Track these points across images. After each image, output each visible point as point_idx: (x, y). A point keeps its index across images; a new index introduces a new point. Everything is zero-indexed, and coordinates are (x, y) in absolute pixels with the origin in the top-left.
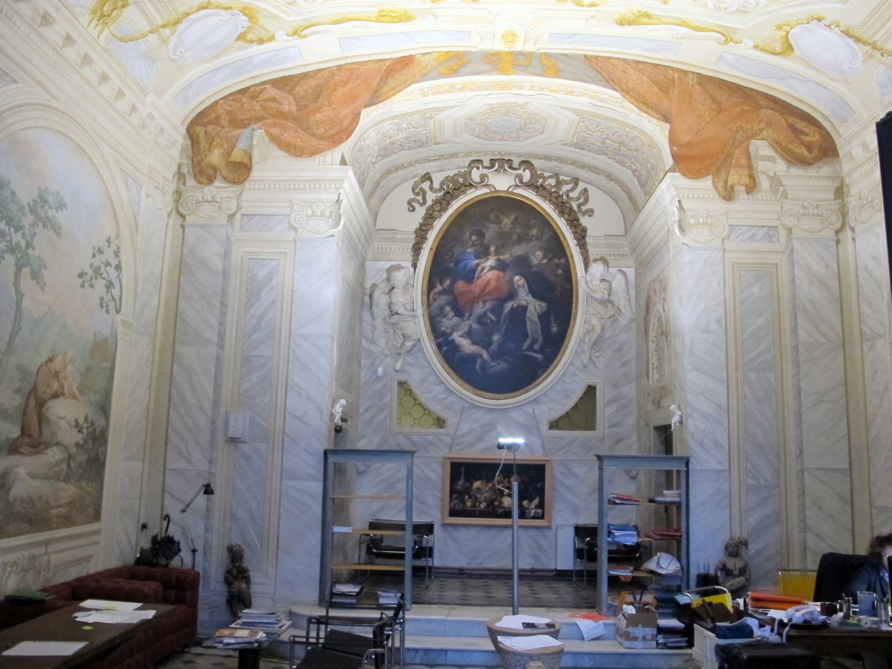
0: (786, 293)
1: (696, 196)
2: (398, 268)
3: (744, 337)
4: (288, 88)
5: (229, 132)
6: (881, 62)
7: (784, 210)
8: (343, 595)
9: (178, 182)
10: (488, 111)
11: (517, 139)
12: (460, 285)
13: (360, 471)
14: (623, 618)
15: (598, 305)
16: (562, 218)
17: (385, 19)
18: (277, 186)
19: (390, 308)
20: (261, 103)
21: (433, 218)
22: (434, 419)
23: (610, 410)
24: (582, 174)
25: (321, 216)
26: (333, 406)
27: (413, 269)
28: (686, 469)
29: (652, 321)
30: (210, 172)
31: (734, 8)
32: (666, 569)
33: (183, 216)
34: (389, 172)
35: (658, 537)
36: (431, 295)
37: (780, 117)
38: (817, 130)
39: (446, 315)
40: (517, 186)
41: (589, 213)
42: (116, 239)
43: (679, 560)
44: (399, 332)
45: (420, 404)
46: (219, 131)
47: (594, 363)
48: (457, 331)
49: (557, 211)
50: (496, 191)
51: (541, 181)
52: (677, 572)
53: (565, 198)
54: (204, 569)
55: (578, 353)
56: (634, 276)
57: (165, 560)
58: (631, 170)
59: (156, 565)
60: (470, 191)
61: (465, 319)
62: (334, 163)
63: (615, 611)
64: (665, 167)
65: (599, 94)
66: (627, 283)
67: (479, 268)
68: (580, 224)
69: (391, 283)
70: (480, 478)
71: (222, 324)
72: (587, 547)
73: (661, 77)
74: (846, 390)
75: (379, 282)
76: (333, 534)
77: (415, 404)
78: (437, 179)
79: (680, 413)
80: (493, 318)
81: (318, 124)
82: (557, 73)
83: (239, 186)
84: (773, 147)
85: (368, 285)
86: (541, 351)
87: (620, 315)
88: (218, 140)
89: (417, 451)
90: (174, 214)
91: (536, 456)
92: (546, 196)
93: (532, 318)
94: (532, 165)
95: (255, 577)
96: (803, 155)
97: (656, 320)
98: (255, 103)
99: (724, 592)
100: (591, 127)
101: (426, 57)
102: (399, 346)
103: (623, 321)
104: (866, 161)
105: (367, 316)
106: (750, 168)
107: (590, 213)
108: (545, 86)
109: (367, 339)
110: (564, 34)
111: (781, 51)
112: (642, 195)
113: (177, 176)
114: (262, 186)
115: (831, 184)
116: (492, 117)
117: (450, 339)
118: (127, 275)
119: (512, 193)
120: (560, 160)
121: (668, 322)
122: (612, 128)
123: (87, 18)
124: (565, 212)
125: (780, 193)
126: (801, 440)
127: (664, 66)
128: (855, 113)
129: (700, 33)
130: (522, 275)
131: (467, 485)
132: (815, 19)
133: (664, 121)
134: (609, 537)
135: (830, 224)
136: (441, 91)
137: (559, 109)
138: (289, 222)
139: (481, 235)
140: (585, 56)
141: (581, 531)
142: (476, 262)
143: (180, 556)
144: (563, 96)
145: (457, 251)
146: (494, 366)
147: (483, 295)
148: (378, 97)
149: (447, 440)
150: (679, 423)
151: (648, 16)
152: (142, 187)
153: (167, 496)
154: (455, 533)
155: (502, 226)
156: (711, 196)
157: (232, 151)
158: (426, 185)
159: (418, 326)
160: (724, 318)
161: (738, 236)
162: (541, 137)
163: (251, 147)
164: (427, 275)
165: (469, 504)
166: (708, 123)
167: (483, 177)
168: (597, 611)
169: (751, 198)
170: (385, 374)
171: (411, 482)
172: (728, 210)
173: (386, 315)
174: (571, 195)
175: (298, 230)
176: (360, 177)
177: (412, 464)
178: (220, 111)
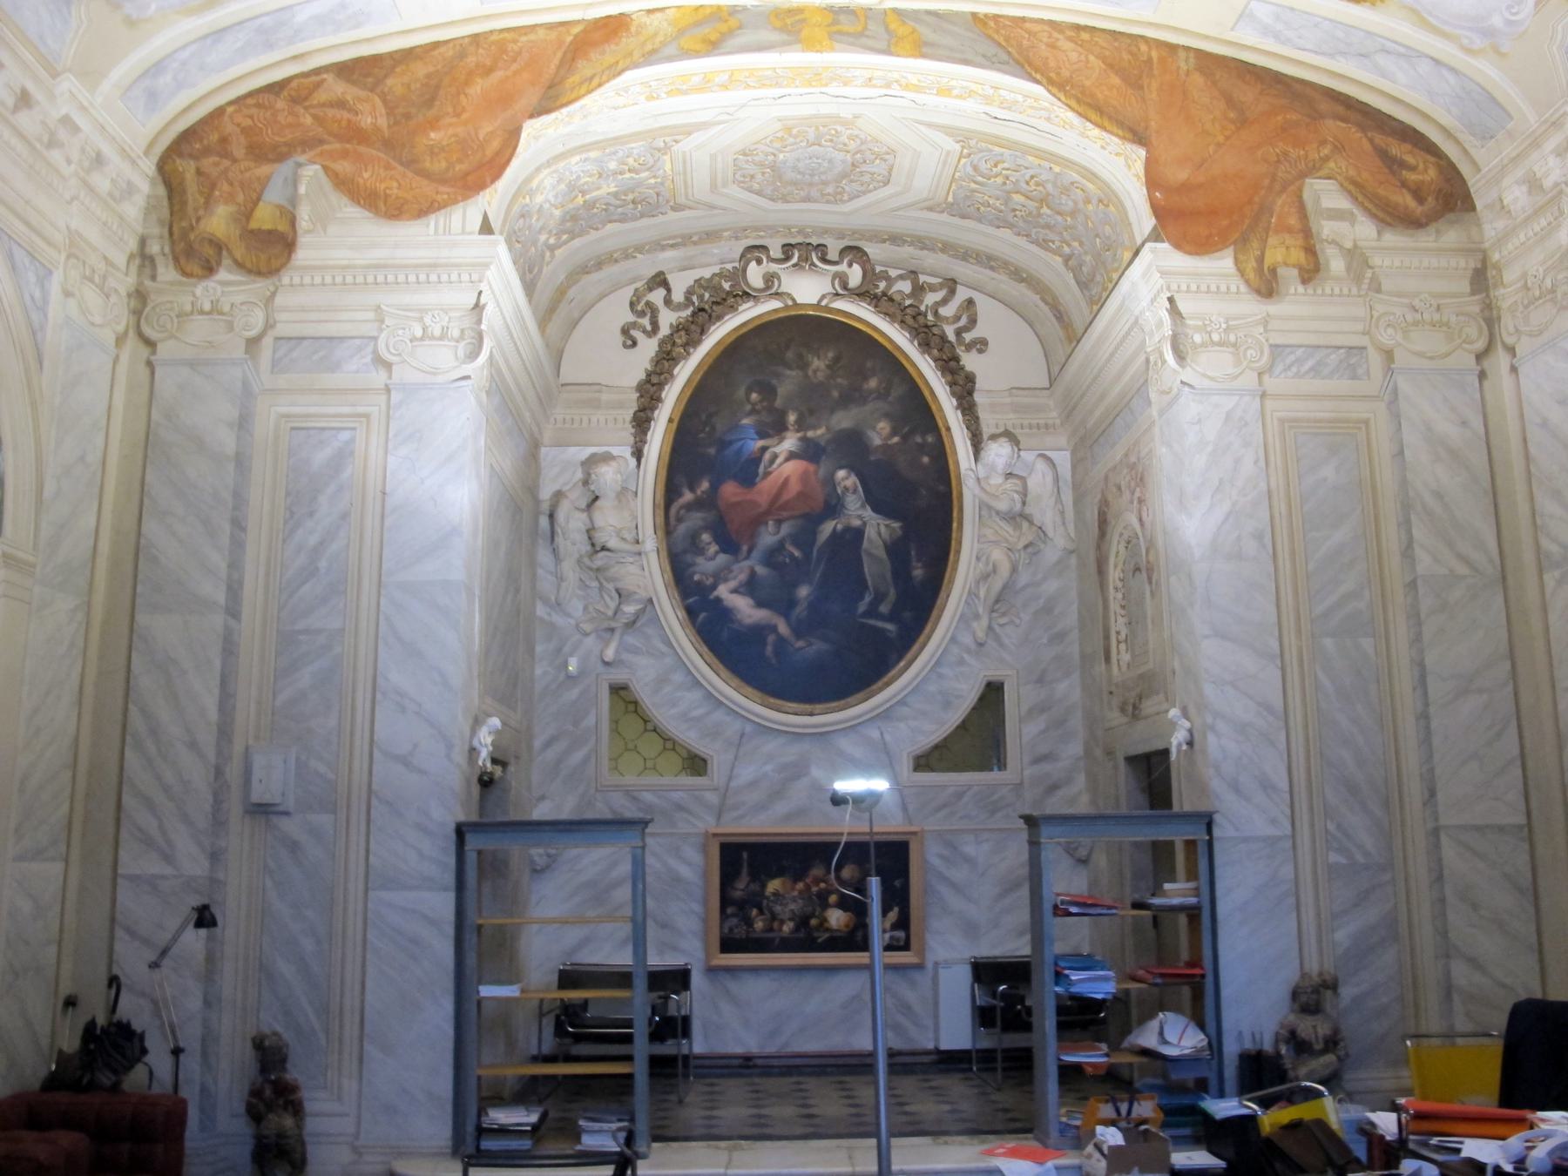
0: (1387, 477)
1: (1204, 288)
2: (607, 458)
3: (1311, 567)
4: (370, 80)
5: (249, 169)
7: (1376, 314)
8: (503, 1131)
9: (139, 275)
10: (779, 135)
11: (837, 198)
12: (730, 490)
13: (539, 868)
14: (1097, 1155)
15: (1003, 524)
16: (926, 356)
19: (590, 538)
20: (312, 111)
21: (673, 359)
22: (683, 759)
23: (1032, 729)
24: (961, 270)
25: (441, 338)
26: (474, 732)
27: (634, 460)
28: (1207, 838)
30: (209, 251)
32: (1177, 1046)
33: (150, 344)
34: (585, 270)
35: (1159, 981)
37: (1359, 135)
38: (1432, 159)
39: (703, 548)
40: (837, 294)
41: (978, 346)
43: (1202, 1026)
44: (610, 586)
45: (655, 730)
47: (998, 639)
48: (726, 580)
49: (916, 343)
50: (796, 304)
51: (882, 285)
52: (1202, 1050)
53: (930, 317)
54: (204, 1090)
55: (965, 620)
56: (1069, 466)
57: (111, 1075)
58: (1060, 256)
59: (92, 1086)
60: (745, 306)
62: (468, 229)
63: (1079, 1139)
64: (1132, 237)
65: (1001, 92)
66: (1057, 479)
67: (767, 456)
68: (962, 368)
69: (592, 488)
70: (780, 873)
71: (235, 565)
72: (1002, 1004)
73: (1126, 56)
75: (567, 488)
76: (479, 1003)
77: (646, 730)
78: (680, 284)
79: (1187, 724)
80: (797, 553)
81: (433, 151)
82: (922, 49)
84: (1350, 192)
85: (546, 494)
86: (892, 617)
88: (226, 187)
89: (651, 821)
90: (132, 341)
91: (890, 824)
92: (894, 313)
93: (874, 551)
94: (865, 254)
95: (316, 1102)
96: (1406, 208)
97: (1123, 544)
98: (302, 111)
99: (1319, 1095)
100: (983, 167)
101: (652, 16)
102: (610, 613)
103: (1051, 555)
105: (544, 556)
106: (1307, 233)
107: (981, 345)
108: (896, 76)
109: (546, 601)
112: (1083, 304)
113: (137, 261)
114: (318, 280)
115: (1462, 263)
116: (788, 149)
117: (712, 597)
119: (828, 309)
120: (922, 243)
121: (1151, 545)
122: (1027, 168)
124: (932, 344)
125: (1367, 281)
126: (1432, 770)
127: (1130, 36)
128: (1509, 115)
130: (851, 468)
131: (754, 887)
133: (1133, 142)
134: (1057, 984)
135: (1464, 341)
136: (684, 87)
137: (922, 128)
138: (375, 352)
139: (768, 391)
140: (974, 15)
141: (985, 972)
142: (761, 443)
143: (146, 1064)
144: (930, 99)
145: (720, 424)
146: (801, 648)
147: (776, 509)
149: (712, 798)
150: (1187, 744)
152: (51, 273)
153: (119, 933)
154: (733, 986)
155: (810, 373)
156: (1233, 289)
157: (252, 210)
158: (657, 296)
159: (647, 573)
160: (1269, 529)
161: (1289, 367)
163: (294, 200)
164: (664, 473)
165: (759, 925)
166: (1219, 145)
167: (770, 279)
168: (1037, 1139)
169: (1310, 291)
170: (582, 672)
171: (641, 886)
172: (1268, 315)
173: (583, 552)
174: (943, 311)
175: (394, 367)
177: (643, 848)
178: (229, 128)
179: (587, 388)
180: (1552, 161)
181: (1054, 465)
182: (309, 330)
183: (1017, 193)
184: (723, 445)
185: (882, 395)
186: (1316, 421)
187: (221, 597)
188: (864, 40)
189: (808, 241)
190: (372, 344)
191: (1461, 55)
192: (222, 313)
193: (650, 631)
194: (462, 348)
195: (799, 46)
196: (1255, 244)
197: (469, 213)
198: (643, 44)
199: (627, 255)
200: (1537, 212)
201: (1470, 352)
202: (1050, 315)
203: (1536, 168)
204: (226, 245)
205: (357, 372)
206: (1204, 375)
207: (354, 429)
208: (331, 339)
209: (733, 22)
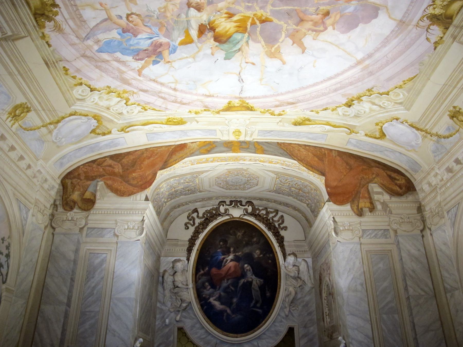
0: (398, 266)
1: (342, 214)
2: (179, 261)
3: (378, 293)
4: (118, 160)
5: (84, 183)
6: (431, 140)
7: (391, 220)
9: (53, 209)
11: (244, 189)
12: (214, 270)
17: (170, 123)
18: (109, 212)
20: (103, 167)
21: (199, 233)
23: (303, 342)
25: (132, 229)
29: (324, 287)
31: (353, 115)
33: (54, 228)
34: (175, 208)
36: (198, 276)
37: (383, 171)
40: (245, 215)
42: (8, 238)
44: (179, 298)
46: (79, 182)
48: (213, 297)
49: (267, 228)
50: (233, 217)
51: (258, 212)
53: (271, 221)
55: (282, 308)
56: (311, 262)
61: (217, 290)
62: (141, 200)
64: (324, 200)
65: (286, 162)
67: (225, 260)
68: (280, 235)
71: (70, 291)
73: (318, 152)
74: (442, 324)
77: (188, 341)
79: (344, 342)
80: (233, 289)
81: (134, 179)
83: (87, 212)
84: (381, 187)
85: (161, 271)
86: (261, 308)
87: (305, 285)
88: (78, 187)
94: (253, 203)
97: (326, 286)
100: (283, 181)
102: (179, 306)
103: (307, 289)
104: (431, 192)
105: (160, 289)
106: (370, 198)
107: (285, 228)
108: (257, 158)
109: (160, 302)
110: (266, 131)
111: (379, 137)
113: (53, 206)
115: (414, 205)
118: (13, 261)
120: (268, 200)
121: (332, 287)
123: (6, 116)
124: (271, 228)
125: (388, 211)
129: (337, 129)
130: (249, 264)
132: (394, 119)
133: (321, 175)
137: (266, 171)
138: (114, 232)
139: (225, 242)
140: (278, 143)
142: (223, 257)
146: (234, 317)
147: (227, 275)
148: (167, 165)
151: (309, 120)
152: (30, 210)
155: (237, 237)
156: (351, 214)
157: (85, 193)
158: (195, 215)
161: (368, 235)
162: (256, 187)
163: (96, 191)
164: (195, 265)
166: (345, 175)
167: (226, 210)
170: (170, 323)
174: (275, 219)
176: (157, 210)
178: (80, 171)
179: (174, 240)
180: (433, 179)
181: (307, 262)
182: (96, 226)
183: (293, 187)
184: (212, 257)
185: (258, 243)
186: (376, 251)
187: (65, 301)
188: (249, 150)
189: (237, 200)
190: (113, 230)
191: (406, 151)
192: (74, 221)
193: (190, 311)
194: (138, 232)
195: (231, 151)
196: (356, 202)
197: (142, 195)
198: (190, 151)
199: (187, 204)
200: (431, 192)
201: (419, 230)
202: (304, 219)
203: (430, 180)
204: (77, 202)
205: (109, 238)
206: (344, 239)
207: (107, 254)
208: (102, 228)
209: (214, 145)
